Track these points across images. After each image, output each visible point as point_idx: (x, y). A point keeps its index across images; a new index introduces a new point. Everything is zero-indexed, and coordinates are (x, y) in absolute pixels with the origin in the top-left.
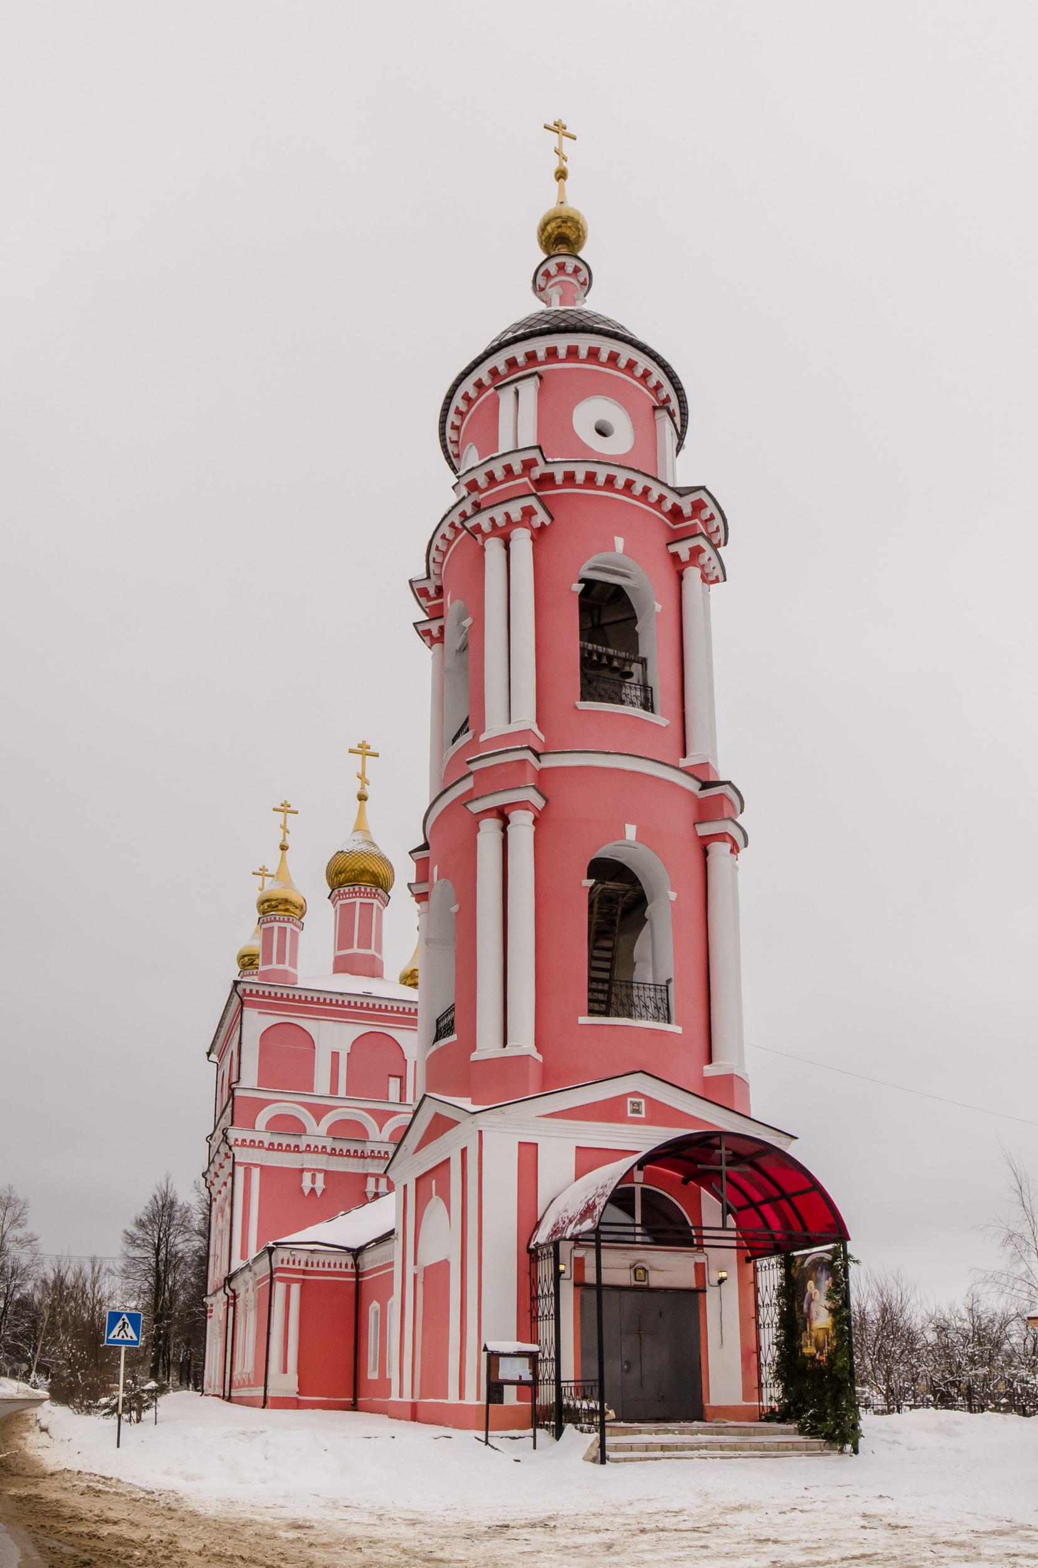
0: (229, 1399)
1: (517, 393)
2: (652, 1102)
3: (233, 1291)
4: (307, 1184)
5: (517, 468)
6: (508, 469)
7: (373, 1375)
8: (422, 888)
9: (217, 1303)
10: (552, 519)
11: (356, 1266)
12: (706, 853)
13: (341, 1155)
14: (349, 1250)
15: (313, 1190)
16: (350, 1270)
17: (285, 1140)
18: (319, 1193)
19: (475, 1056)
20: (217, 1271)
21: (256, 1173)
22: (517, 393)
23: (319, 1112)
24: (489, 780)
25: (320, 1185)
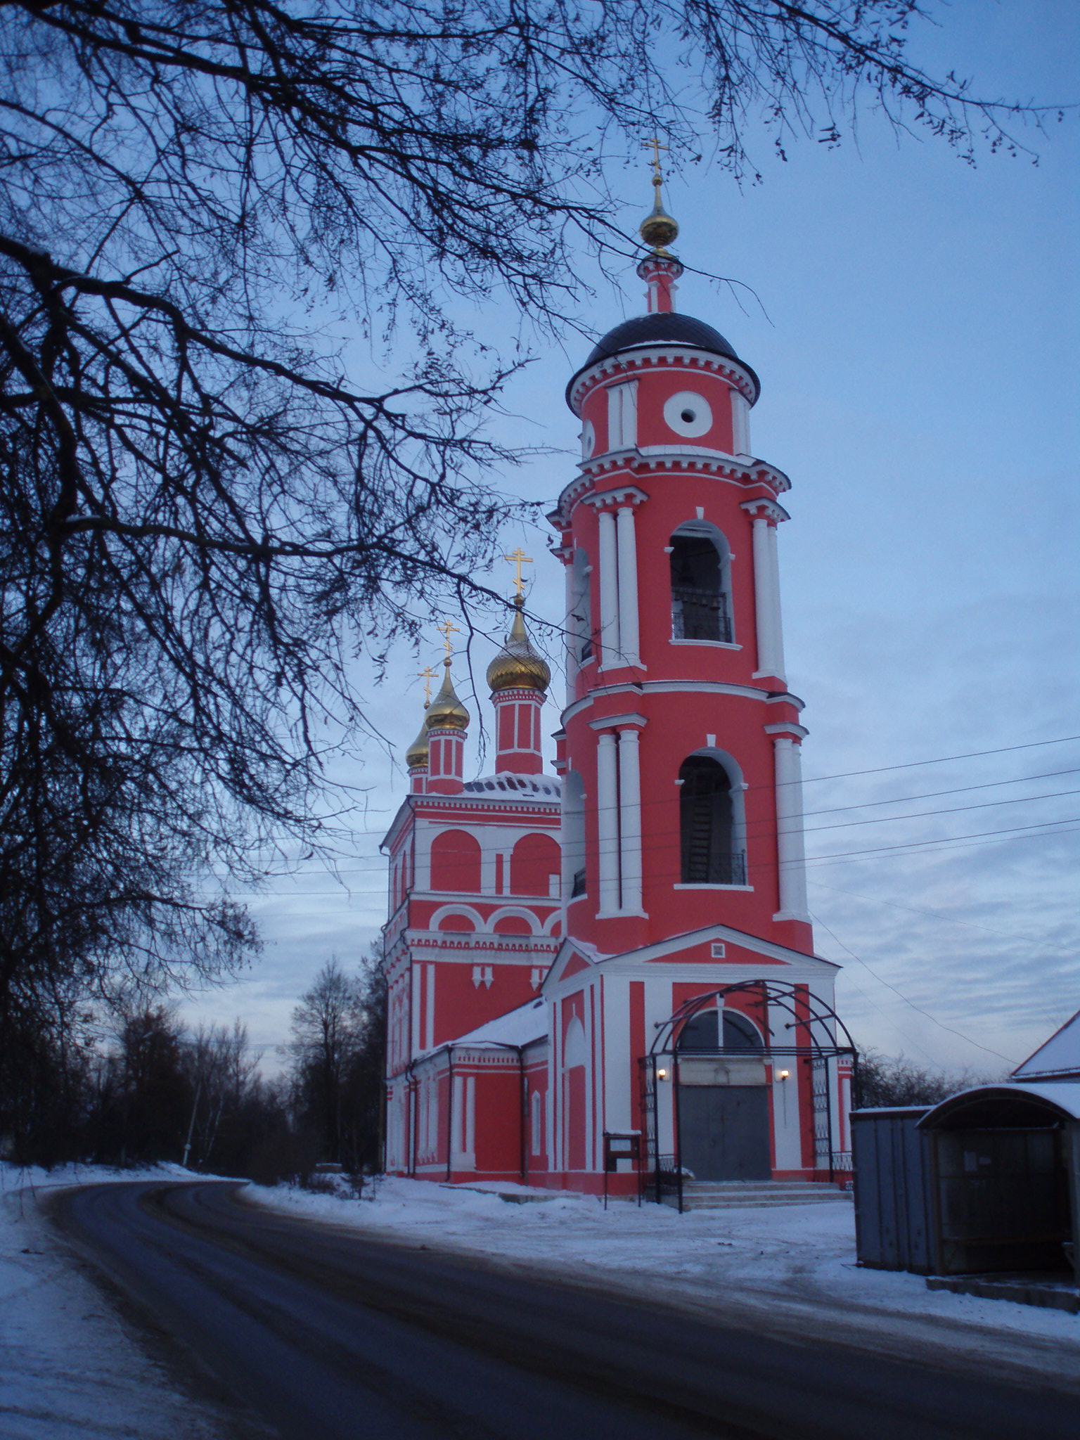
0: (413, 1176)
1: (621, 392)
2: (730, 946)
3: (414, 1077)
4: (477, 976)
5: (620, 463)
6: (614, 463)
7: (536, 1152)
8: (563, 765)
9: (398, 1088)
10: (648, 496)
11: (521, 1060)
12: (774, 745)
13: (507, 950)
14: (512, 1048)
15: (483, 983)
16: (515, 1063)
17: (456, 939)
18: (488, 985)
19: (598, 917)
20: (397, 1057)
23: (486, 911)
24: (606, 706)
25: (489, 977)
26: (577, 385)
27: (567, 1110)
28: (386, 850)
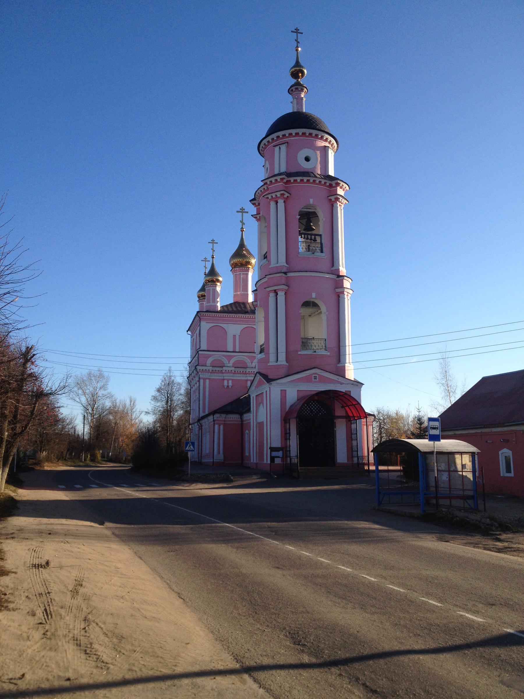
1: (280, 148)
3: (201, 424)
7: (247, 454)
15: (228, 386)
18: (230, 387)
21: (207, 381)
22: (280, 148)
26: (262, 145)
27: (265, 433)
28: (189, 332)
